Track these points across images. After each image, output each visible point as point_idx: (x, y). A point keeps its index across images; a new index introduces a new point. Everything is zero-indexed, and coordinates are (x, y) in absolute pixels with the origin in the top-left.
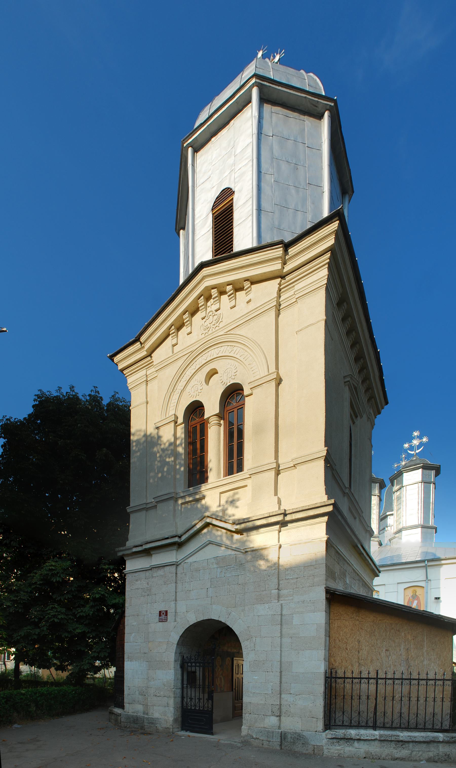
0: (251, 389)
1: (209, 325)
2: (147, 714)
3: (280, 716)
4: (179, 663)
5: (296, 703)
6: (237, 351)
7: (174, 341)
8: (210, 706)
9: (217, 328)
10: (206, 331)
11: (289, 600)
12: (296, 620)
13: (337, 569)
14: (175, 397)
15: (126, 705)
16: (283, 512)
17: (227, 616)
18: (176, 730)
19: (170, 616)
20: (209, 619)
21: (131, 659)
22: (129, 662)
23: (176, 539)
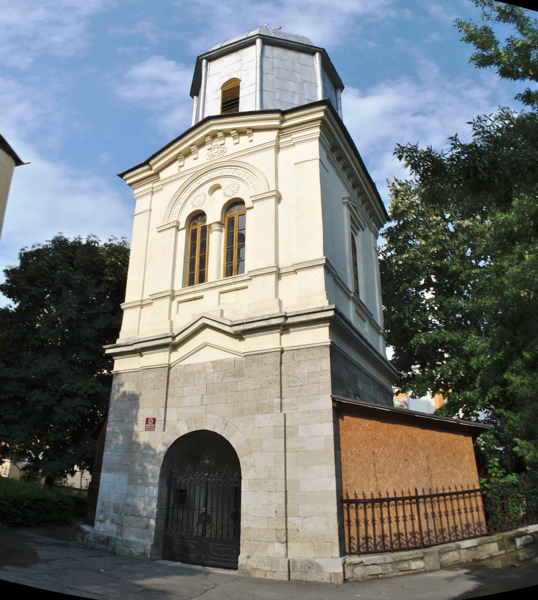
0: (252, 201)
1: (214, 154)
2: (121, 536)
3: (287, 542)
4: (166, 479)
5: (306, 527)
6: (239, 172)
7: (181, 164)
8: (200, 531)
9: (221, 156)
10: (212, 158)
11: (293, 409)
12: (302, 432)
13: (345, 375)
14: (179, 206)
15: (97, 524)
16: (283, 314)
17: (223, 427)
18: (156, 557)
19: (159, 425)
20: (202, 430)
21: (109, 470)
22: (106, 474)
23: (169, 340)
